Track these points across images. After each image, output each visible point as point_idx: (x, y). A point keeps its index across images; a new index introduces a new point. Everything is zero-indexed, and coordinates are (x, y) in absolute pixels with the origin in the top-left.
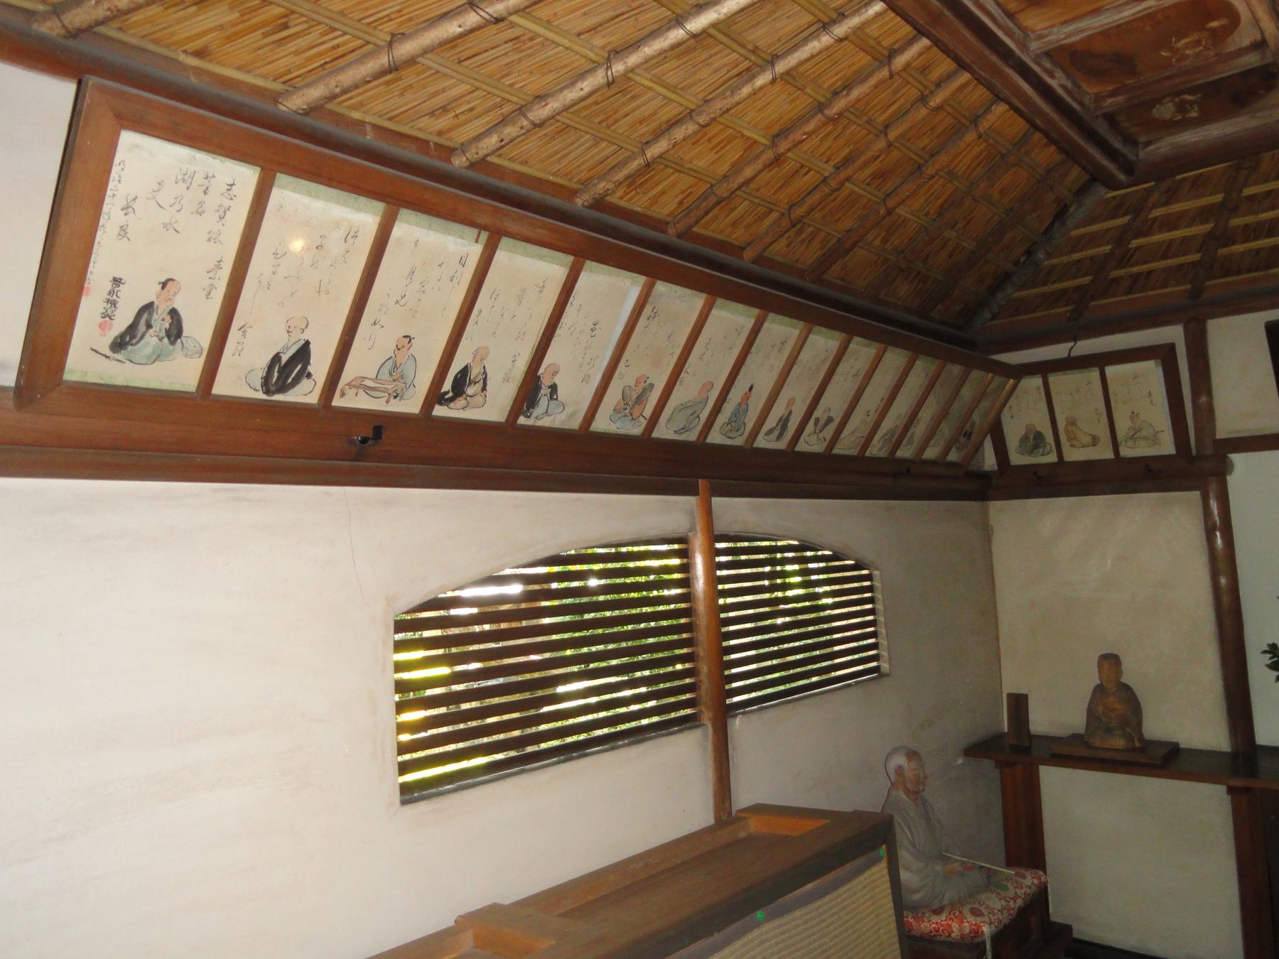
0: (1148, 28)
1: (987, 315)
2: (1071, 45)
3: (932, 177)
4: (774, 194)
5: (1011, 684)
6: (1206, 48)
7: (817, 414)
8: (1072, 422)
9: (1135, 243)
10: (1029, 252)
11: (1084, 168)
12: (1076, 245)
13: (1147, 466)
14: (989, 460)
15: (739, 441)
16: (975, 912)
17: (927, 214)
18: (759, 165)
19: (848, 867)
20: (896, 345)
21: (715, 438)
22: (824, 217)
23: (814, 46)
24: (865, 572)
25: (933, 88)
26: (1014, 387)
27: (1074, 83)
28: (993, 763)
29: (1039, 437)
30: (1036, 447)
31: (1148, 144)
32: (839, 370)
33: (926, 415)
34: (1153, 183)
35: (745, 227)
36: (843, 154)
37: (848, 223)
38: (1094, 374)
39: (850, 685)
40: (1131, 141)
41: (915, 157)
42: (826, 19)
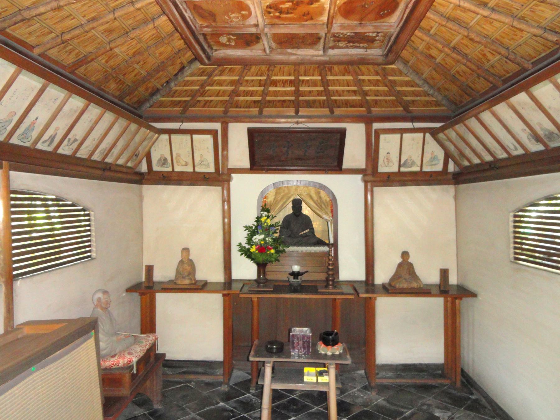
0: (222, 6)
3: (132, 39)
4: (54, 24)
5: (146, 262)
6: (240, 21)
7: (70, 136)
8: (178, 155)
9: (207, 88)
10: (168, 82)
11: (193, 53)
12: (186, 83)
13: (204, 176)
14: (144, 168)
15: (27, 144)
16: (130, 354)
17: (128, 55)
18: (49, 7)
19: (77, 342)
20: (111, 111)
21: (14, 140)
22: (79, 43)
24: (86, 213)
26: (157, 138)
27: (194, 17)
28: (138, 294)
29: (165, 160)
30: (164, 164)
31: (216, 50)
32: (83, 117)
33: (121, 144)
34: (216, 66)
35: (37, 37)
36: (93, 15)
37: (90, 49)
38: (188, 137)
39: (77, 264)
40: (210, 47)
41: (126, 28)
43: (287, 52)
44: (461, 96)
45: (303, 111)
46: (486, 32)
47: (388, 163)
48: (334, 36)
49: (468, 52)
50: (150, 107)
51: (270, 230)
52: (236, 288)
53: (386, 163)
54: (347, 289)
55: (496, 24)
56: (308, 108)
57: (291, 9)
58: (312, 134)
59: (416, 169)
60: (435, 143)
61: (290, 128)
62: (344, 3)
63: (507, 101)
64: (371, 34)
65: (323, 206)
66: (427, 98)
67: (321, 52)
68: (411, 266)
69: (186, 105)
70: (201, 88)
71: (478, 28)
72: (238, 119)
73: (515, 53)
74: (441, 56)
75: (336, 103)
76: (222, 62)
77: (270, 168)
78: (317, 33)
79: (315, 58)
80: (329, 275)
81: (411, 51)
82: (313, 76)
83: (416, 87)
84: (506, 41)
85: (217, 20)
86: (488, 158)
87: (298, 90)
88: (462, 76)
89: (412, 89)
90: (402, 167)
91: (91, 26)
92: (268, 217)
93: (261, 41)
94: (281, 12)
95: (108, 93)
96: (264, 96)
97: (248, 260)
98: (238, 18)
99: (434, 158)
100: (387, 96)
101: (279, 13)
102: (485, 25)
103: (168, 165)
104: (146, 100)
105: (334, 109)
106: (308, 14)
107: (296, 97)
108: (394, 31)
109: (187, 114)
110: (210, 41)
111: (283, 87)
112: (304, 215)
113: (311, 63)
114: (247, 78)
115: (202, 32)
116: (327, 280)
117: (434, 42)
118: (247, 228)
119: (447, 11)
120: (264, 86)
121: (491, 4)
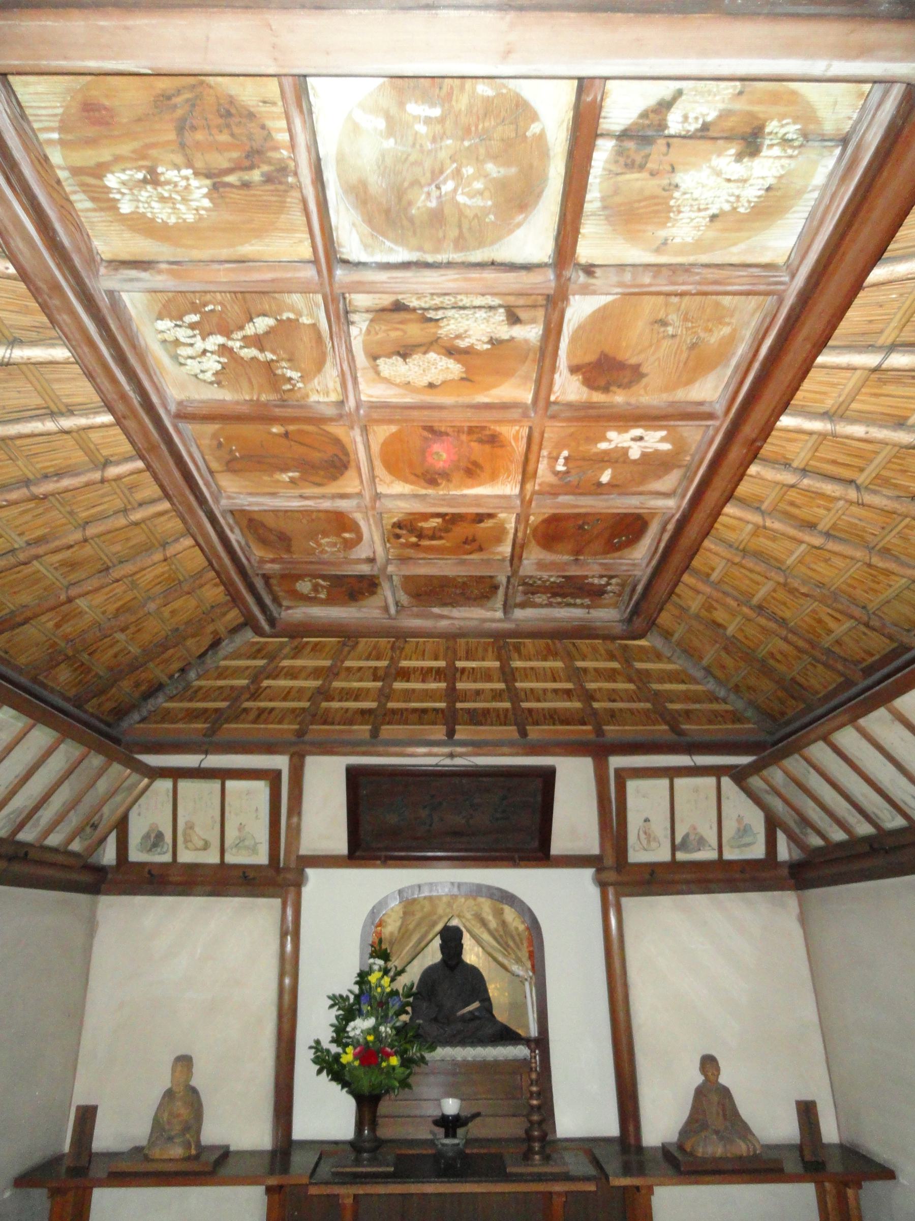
0: (304, 521)
1: (136, 717)
2: (249, 512)
3: (117, 581)
5: (80, 1098)
8: (190, 826)
9: (266, 683)
10: (183, 670)
12: (222, 674)
14: (109, 855)
17: (104, 613)
23: (36, 426)
25: (136, 505)
27: (247, 544)
29: (160, 836)
30: (155, 845)
31: (288, 608)
34: (286, 639)
36: (39, 533)
37: (25, 598)
38: (216, 785)
40: (276, 600)
42: (55, 410)
43: (432, 613)
44: (782, 702)
45: (462, 732)
46: (818, 578)
47: (649, 842)
48: (524, 584)
49: (787, 614)
50: (140, 722)
51: (390, 1004)
52: (301, 1163)
53: (645, 842)
54: (577, 1164)
55: (838, 562)
56: (475, 724)
57: (440, 530)
58: (484, 779)
59: (711, 855)
60: (743, 796)
61: (437, 765)
62: (544, 521)
63: (889, 705)
64: (596, 581)
65: (511, 943)
66: (715, 706)
67: (499, 614)
68: (725, 1093)
69: (217, 718)
70: (252, 682)
71: (803, 569)
72: (327, 748)
73: (880, 617)
74: (735, 623)
75: (531, 715)
76: (298, 631)
77: (396, 854)
78: (491, 577)
79: (487, 625)
80: (531, 1122)
81: (676, 612)
82: (483, 660)
83: (690, 683)
84: (859, 593)
85: (293, 549)
86: (864, 829)
87: (454, 689)
88: (778, 661)
89: (682, 687)
90: (679, 849)
91: (34, 551)
92: (386, 971)
93: (379, 591)
94: (420, 536)
95: (52, 691)
96: (383, 700)
97: (335, 1087)
98: (335, 545)
99: (744, 830)
100: (634, 701)
101: (416, 537)
102: (816, 563)
103: (164, 850)
104: (133, 707)
105: (528, 727)
106: (474, 540)
107: (448, 703)
108: (643, 574)
109: (217, 738)
110: (276, 588)
111: (423, 681)
112: (467, 965)
113: (481, 634)
114: (348, 663)
115: (260, 572)
116: (529, 1138)
117: (720, 595)
118: (337, 1000)
119: (741, 538)
120: (383, 680)
121: (824, 525)
